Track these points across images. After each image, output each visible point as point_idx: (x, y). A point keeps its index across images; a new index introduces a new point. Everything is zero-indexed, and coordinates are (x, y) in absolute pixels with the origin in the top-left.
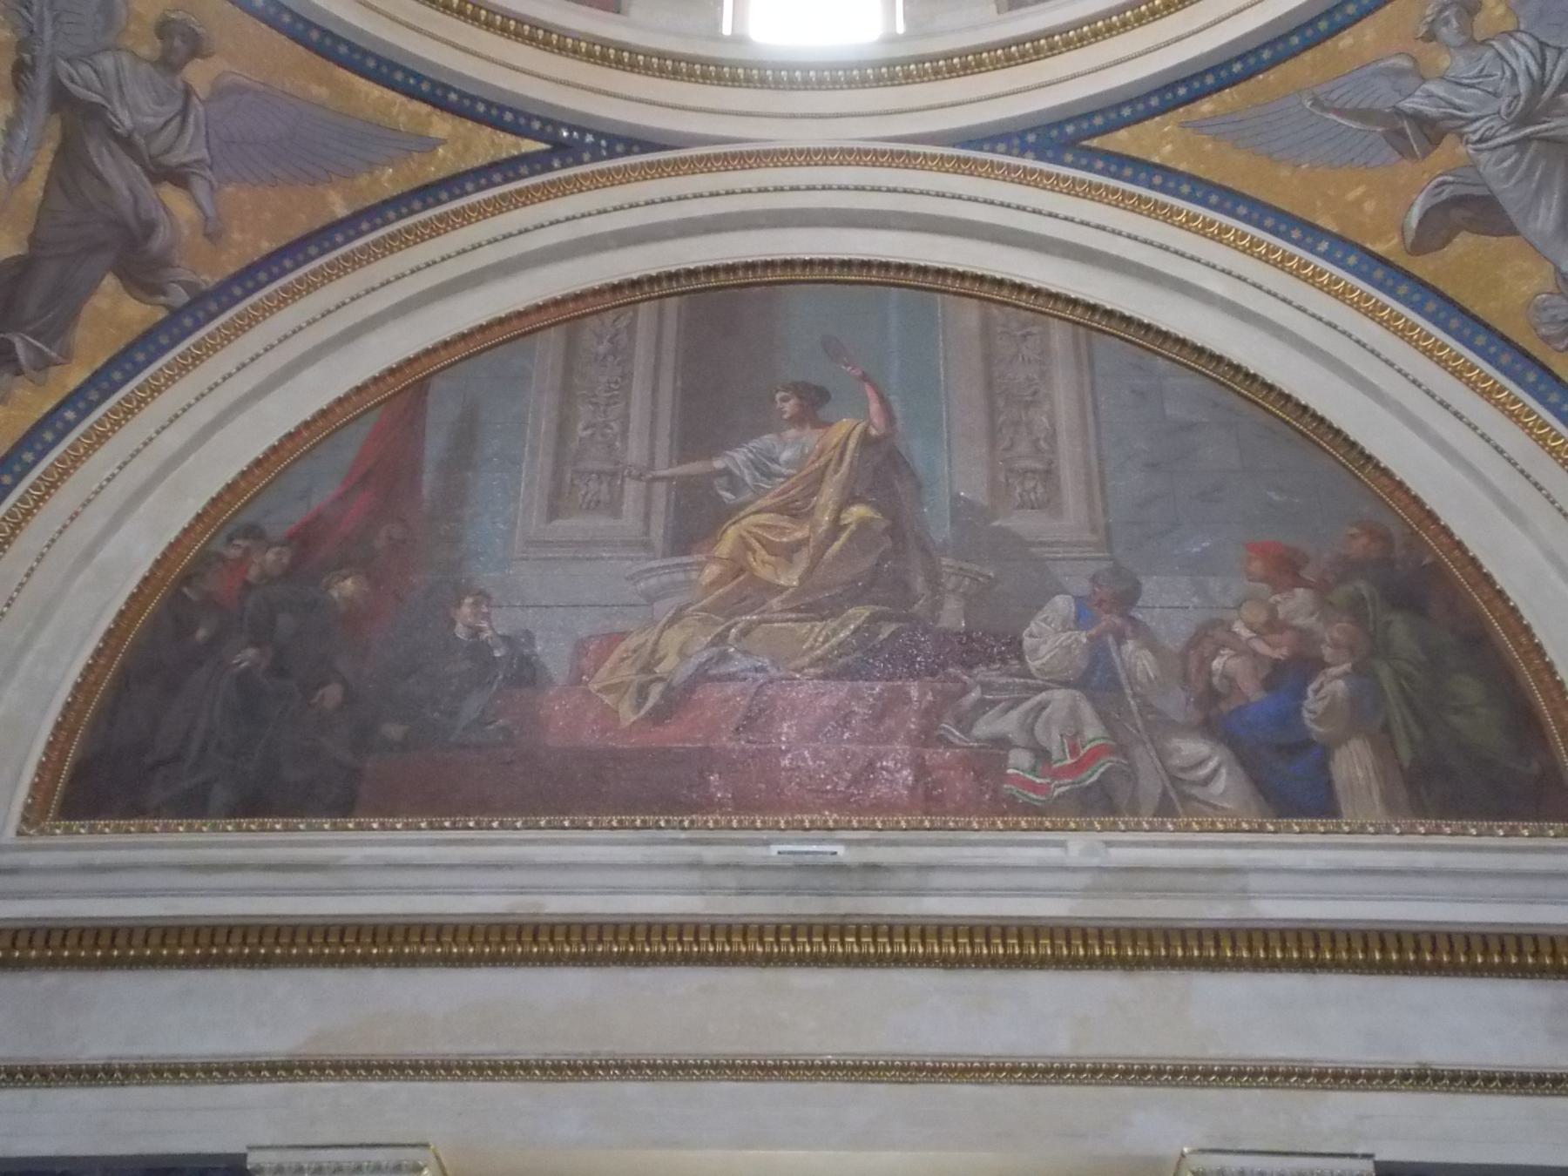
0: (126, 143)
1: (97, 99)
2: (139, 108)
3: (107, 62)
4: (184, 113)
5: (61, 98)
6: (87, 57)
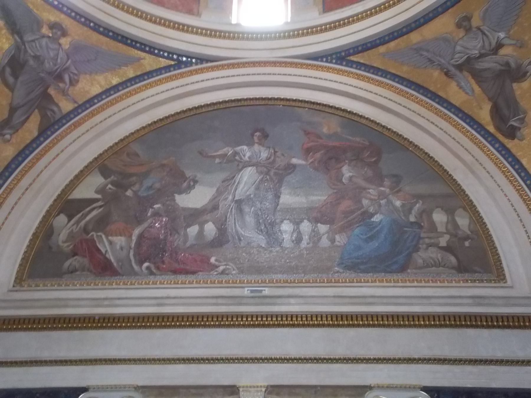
0: (482, 56)
1: (466, 57)
2: (474, 46)
3: (458, 48)
4: (484, 34)
5: (460, 67)
6: (454, 53)
